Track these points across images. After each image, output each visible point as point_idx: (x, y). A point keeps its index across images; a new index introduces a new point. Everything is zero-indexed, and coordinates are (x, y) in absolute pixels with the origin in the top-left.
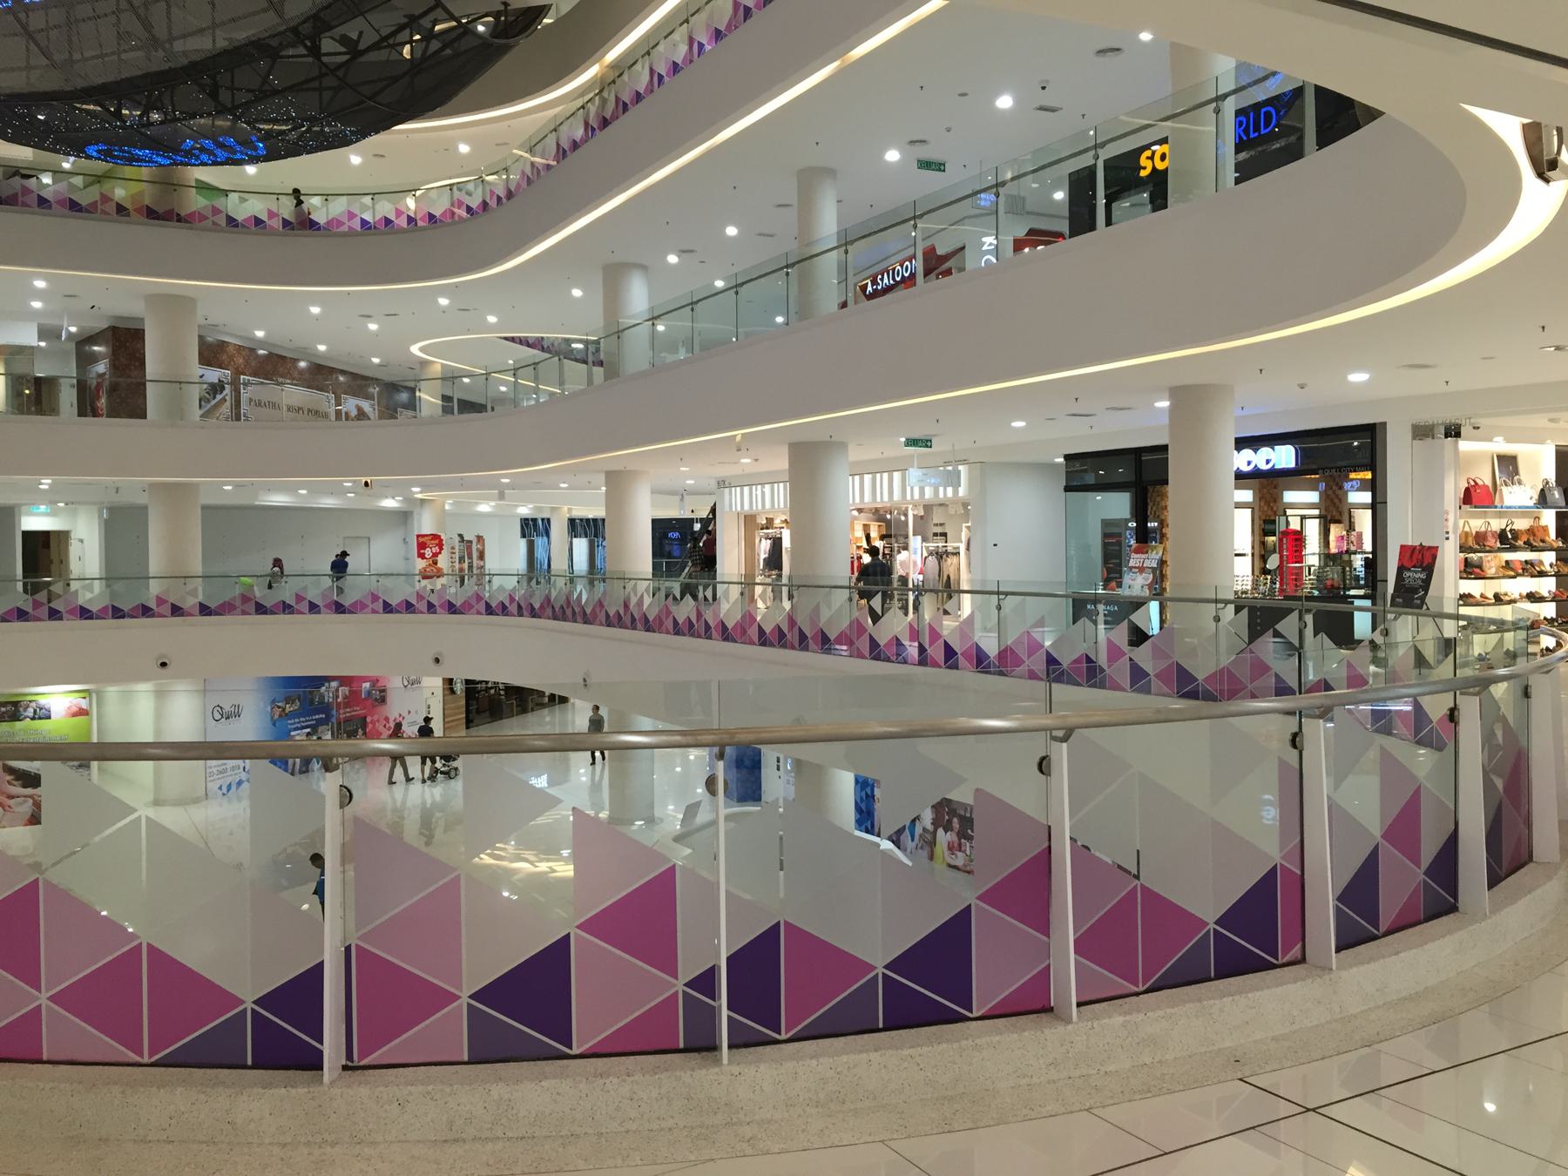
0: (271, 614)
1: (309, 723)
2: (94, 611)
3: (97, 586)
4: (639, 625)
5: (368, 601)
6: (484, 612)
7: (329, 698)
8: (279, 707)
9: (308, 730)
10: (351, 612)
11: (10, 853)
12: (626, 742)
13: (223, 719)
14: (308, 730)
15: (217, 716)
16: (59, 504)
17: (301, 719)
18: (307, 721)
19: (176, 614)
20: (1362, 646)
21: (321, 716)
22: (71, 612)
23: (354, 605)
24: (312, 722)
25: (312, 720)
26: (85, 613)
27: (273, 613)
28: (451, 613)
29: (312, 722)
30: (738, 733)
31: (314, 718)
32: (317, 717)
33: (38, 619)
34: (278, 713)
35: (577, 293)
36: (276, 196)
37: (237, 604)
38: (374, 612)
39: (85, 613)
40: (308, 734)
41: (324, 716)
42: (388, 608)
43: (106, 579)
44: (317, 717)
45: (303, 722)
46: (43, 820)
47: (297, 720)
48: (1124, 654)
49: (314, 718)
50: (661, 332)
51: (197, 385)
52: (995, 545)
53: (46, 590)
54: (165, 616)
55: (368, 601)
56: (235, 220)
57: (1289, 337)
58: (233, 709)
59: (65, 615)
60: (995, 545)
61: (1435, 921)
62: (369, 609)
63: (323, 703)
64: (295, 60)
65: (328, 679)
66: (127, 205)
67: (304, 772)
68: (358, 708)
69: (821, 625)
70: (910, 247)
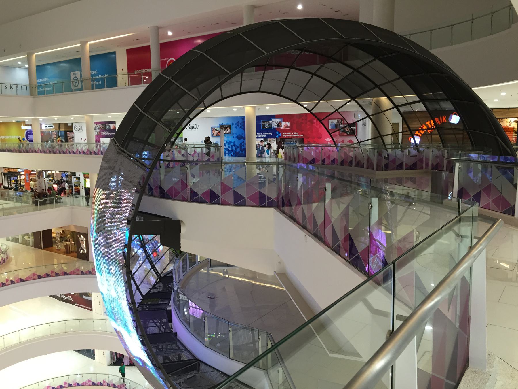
1: (263, 136)
4: (71, 153)
5: (88, 382)
7: (274, 125)
8: (217, 130)
9: (262, 139)
11: (429, 369)
13: (190, 129)
14: (262, 139)
18: (260, 135)
21: (270, 134)
24: (264, 136)
25: (264, 135)
29: (264, 136)
31: (265, 134)
32: (267, 134)
34: (216, 133)
35: (300, 7)
40: (262, 141)
41: (271, 134)
44: (267, 134)
45: (259, 135)
46: (74, 171)
47: (261, 134)
48: (482, 190)
49: (265, 134)
53: (153, 349)
54: (36, 279)
55: (88, 382)
56: (67, 273)
58: (194, 126)
61: (6, 122)
63: (271, 127)
65: (274, 117)
67: (259, 157)
68: (298, 133)
69: (83, 150)
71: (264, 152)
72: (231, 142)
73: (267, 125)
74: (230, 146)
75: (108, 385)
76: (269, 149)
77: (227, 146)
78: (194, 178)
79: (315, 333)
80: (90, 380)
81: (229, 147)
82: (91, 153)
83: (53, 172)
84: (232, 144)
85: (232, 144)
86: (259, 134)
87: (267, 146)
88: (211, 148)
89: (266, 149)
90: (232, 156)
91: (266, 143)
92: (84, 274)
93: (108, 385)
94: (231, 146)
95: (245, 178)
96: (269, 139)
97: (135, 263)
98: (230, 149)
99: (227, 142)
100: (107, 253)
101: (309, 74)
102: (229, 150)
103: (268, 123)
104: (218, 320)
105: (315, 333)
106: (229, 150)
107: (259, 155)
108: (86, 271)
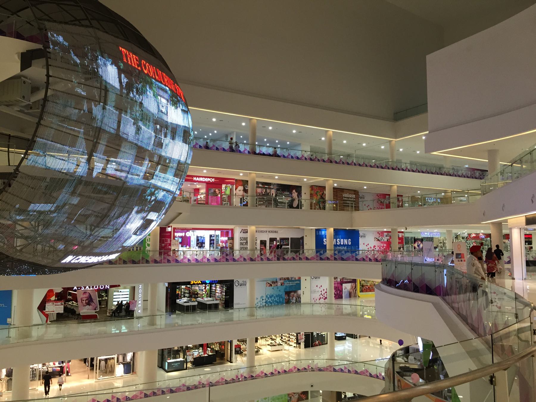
2: (136, 261)
6: (276, 260)
10: (346, 260)
12: (172, 376)
13: (239, 286)
20: (175, 387)
22: (221, 149)
23: (347, 258)
26: (307, 259)
27: (324, 260)
37: (350, 258)
38: (330, 371)
39: (307, 259)
42: (335, 370)
51: (166, 379)
52: (306, 280)
56: (343, 259)
57: (528, 134)
59: (303, 259)
60: (306, 280)
62: (329, 370)
73: (294, 298)
75: (313, 370)
77: (276, 299)
79: (14, 33)
80: (223, 378)
81: (278, 299)
82: (331, 162)
88: (360, 202)
92: (358, 261)
93: (313, 370)
98: (278, 301)
100: (481, 175)
101: (452, 376)
103: (295, 295)
104: (9, 336)
105: (14, 33)
106: (277, 302)
108: (360, 258)
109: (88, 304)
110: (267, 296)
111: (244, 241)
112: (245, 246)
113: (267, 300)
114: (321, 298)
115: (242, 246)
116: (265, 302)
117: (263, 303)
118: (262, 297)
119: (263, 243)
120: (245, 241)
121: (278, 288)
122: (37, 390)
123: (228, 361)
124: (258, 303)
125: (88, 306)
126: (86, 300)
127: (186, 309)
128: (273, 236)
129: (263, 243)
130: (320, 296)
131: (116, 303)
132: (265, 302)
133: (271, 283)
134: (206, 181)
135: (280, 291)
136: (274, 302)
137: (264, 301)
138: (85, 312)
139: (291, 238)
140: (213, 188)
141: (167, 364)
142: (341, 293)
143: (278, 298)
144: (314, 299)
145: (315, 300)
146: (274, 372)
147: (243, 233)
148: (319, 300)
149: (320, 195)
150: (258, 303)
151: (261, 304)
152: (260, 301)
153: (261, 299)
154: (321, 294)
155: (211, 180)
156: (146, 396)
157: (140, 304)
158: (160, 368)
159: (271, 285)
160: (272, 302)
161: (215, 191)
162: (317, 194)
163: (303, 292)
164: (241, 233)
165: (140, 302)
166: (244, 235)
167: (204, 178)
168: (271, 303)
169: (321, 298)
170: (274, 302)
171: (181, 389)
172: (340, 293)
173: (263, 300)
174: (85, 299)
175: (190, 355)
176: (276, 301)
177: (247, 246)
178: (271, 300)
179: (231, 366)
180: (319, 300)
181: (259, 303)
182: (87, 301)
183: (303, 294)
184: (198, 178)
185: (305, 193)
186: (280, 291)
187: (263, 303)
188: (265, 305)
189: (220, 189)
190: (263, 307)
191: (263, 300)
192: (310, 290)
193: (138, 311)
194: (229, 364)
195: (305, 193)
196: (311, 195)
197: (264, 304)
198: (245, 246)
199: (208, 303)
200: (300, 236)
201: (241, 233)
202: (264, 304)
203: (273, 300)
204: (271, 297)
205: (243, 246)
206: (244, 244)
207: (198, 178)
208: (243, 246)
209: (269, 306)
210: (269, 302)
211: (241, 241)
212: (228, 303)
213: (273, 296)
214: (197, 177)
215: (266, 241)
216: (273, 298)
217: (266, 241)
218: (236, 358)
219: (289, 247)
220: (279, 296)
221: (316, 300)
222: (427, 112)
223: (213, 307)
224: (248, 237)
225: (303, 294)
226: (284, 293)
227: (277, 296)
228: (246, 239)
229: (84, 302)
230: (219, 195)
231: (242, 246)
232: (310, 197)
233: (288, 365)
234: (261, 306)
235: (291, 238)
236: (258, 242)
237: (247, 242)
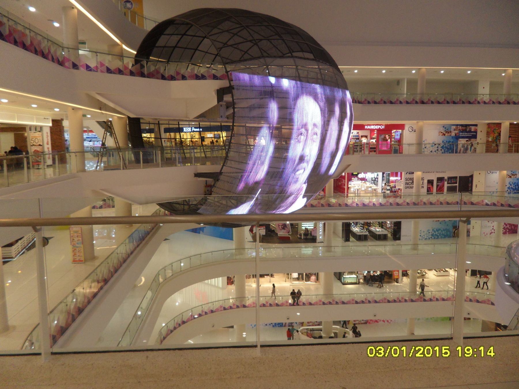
0: (113, 74)
3: (488, 96)
5: (285, 303)
8: (442, 133)
9: (467, 139)
15: (411, 130)
16: (201, 225)
17: (466, 133)
18: (468, 134)
19: (75, 68)
25: (470, 134)
28: (109, 73)
30: (513, 133)
31: (471, 134)
33: (178, 80)
36: (382, 294)
40: (467, 141)
43: (489, 95)
49: (471, 134)
50: (414, 73)
55: (285, 303)
59: (371, 103)
64: (457, 249)
66: (426, 202)
67: (464, 153)
70: (193, 49)
71: (468, 149)
72: (450, 142)
74: (514, 185)
76: (471, 147)
78: (201, 74)
81: (514, 187)
83: (27, 32)
84: (516, 184)
85: (516, 184)
86: (467, 134)
87: (471, 145)
89: (469, 147)
90: (450, 153)
91: (470, 142)
94: (450, 145)
95: (213, 55)
96: (472, 140)
97: (282, 208)
98: (514, 188)
99: (512, 183)
102: (448, 149)
107: (465, 152)
109: (283, 228)
110: (433, 230)
111: (409, 181)
112: (410, 186)
113: (433, 234)
114: (492, 232)
115: (407, 186)
116: (431, 235)
117: (429, 235)
118: (429, 230)
119: (430, 182)
120: (412, 181)
121: (445, 223)
122: (252, 286)
123: (395, 281)
124: (424, 236)
125: (283, 230)
126: (282, 226)
127: (360, 238)
128: (440, 175)
129: (430, 182)
130: (491, 230)
131: (304, 228)
132: (431, 235)
133: (445, 133)
134: (377, 128)
135: (448, 225)
136: (441, 235)
137: (430, 234)
138: (281, 235)
139: (459, 177)
140: (382, 134)
141: (343, 278)
142: (516, 228)
143: (445, 232)
144: (484, 233)
145: (486, 234)
146: (432, 298)
147: (409, 174)
148: (490, 234)
149: (498, 132)
150: (424, 236)
151: (427, 236)
152: (426, 234)
153: (427, 232)
154: (493, 229)
155: (382, 127)
156: (324, 304)
157: (321, 232)
158: (338, 280)
159: (511, 177)
160: (438, 235)
161: (385, 137)
162: (494, 132)
163: (473, 226)
164: (406, 174)
165: (321, 230)
166: (410, 176)
167: (374, 126)
168: (438, 236)
169: (492, 232)
170: (441, 235)
171: (351, 302)
172: (514, 228)
173: (429, 233)
174: (281, 225)
175: (361, 274)
176: (443, 234)
177: (413, 186)
178: (438, 233)
179: (397, 286)
180: (490, 234)
181: (426, 236)
182: (282, 227)
183: (473, 228)
184: (369, 126)
185: (481, 131)
186: (448, 225)
187: (429, 235)
188: (431, 237)
189: (390, 135)
190: (429, 239)
191: (429, 233)
192: (480, 225)
193: (320, 237)
194: (396, 284)
195: (481, 131)
196: (488, 134)
197: (430, 236)
198: (410, 186)
199: (378, 233)
200: (468, 175)
201: (406, 174)
202: (430, 236)
203: (440, 233)
204: (438, 230)
205: (408, 186)
206: (410, 183)
207: (369, 126)
208: (408, 186)
209: (435, 238)
210: (436, 235)
211: (406, 182)
212: (396, 234)
213: (439, 229)
214: (368, 125)
215: (433, 180)
216: (440, 232)
217: (433, 180)
218: (402, 279)
219: (457, 185)
220: (447, 230)
221: (487, 234)
222: (136, 163)
223: (384, 238)
224: (414, 177)
225: (473, 228)
226: (452, 227)
227: (444, 230)
228: (412, 179)
229: (281, 227)
230: (389, 140)
231: (407, 186)
232: (487, 134)
233: (447, 294)
234: (428, 238)
235: (459, 177)
236: (426, 182)
237: (413, 182)
